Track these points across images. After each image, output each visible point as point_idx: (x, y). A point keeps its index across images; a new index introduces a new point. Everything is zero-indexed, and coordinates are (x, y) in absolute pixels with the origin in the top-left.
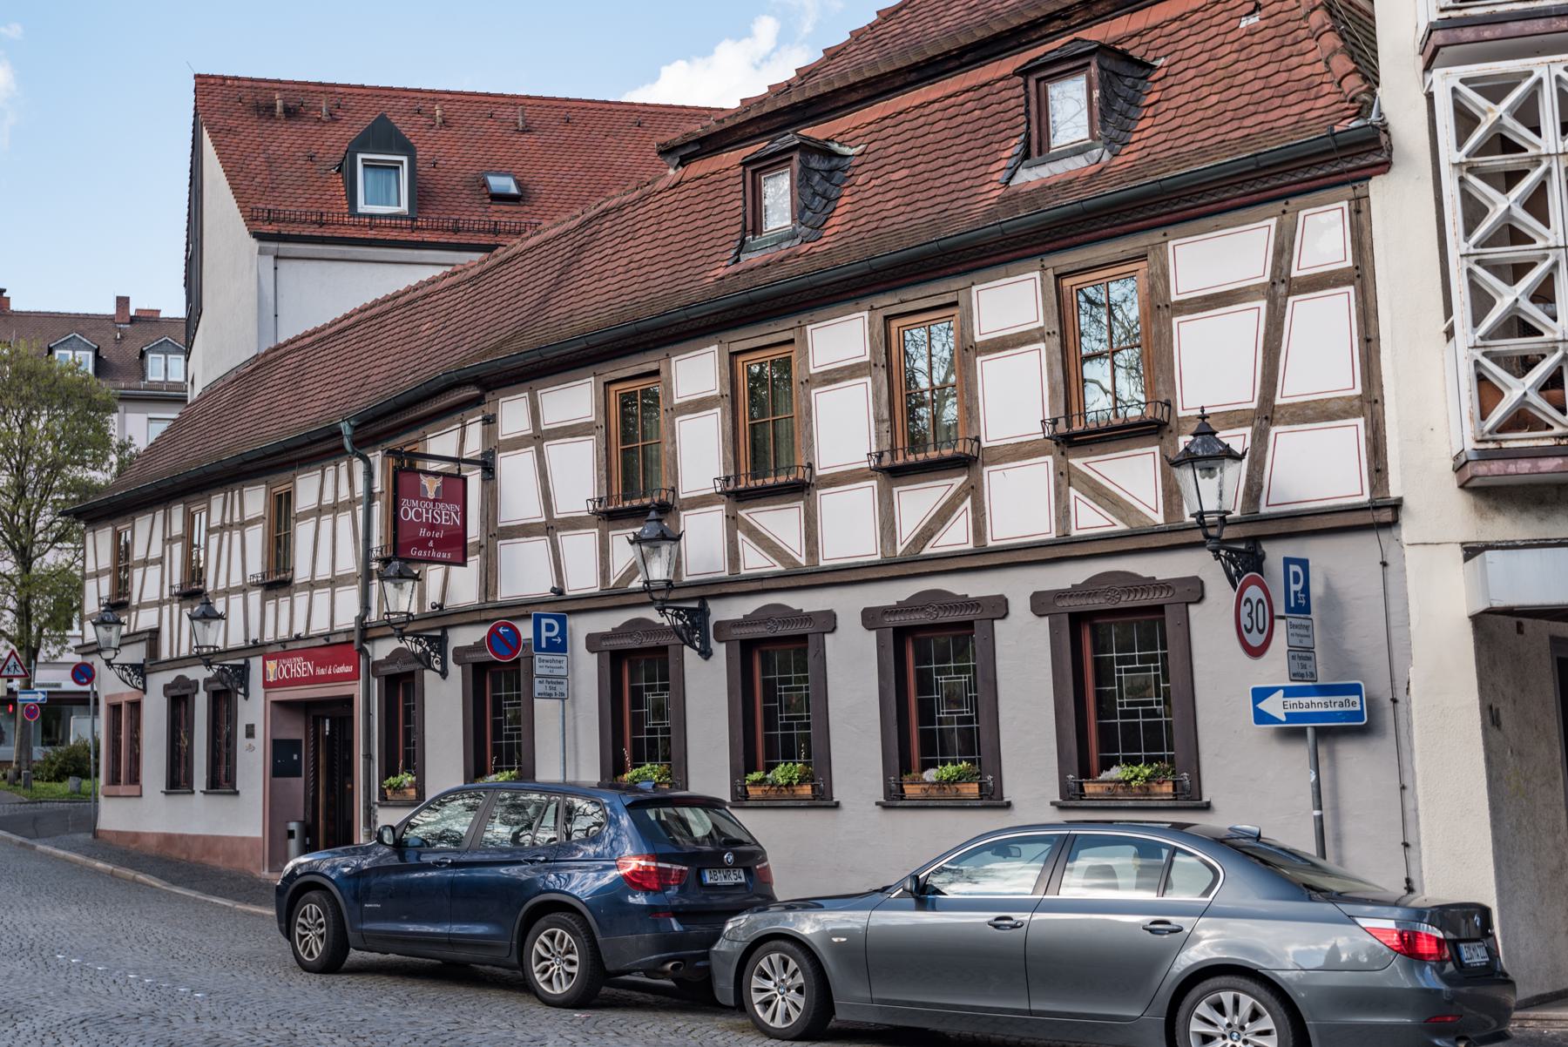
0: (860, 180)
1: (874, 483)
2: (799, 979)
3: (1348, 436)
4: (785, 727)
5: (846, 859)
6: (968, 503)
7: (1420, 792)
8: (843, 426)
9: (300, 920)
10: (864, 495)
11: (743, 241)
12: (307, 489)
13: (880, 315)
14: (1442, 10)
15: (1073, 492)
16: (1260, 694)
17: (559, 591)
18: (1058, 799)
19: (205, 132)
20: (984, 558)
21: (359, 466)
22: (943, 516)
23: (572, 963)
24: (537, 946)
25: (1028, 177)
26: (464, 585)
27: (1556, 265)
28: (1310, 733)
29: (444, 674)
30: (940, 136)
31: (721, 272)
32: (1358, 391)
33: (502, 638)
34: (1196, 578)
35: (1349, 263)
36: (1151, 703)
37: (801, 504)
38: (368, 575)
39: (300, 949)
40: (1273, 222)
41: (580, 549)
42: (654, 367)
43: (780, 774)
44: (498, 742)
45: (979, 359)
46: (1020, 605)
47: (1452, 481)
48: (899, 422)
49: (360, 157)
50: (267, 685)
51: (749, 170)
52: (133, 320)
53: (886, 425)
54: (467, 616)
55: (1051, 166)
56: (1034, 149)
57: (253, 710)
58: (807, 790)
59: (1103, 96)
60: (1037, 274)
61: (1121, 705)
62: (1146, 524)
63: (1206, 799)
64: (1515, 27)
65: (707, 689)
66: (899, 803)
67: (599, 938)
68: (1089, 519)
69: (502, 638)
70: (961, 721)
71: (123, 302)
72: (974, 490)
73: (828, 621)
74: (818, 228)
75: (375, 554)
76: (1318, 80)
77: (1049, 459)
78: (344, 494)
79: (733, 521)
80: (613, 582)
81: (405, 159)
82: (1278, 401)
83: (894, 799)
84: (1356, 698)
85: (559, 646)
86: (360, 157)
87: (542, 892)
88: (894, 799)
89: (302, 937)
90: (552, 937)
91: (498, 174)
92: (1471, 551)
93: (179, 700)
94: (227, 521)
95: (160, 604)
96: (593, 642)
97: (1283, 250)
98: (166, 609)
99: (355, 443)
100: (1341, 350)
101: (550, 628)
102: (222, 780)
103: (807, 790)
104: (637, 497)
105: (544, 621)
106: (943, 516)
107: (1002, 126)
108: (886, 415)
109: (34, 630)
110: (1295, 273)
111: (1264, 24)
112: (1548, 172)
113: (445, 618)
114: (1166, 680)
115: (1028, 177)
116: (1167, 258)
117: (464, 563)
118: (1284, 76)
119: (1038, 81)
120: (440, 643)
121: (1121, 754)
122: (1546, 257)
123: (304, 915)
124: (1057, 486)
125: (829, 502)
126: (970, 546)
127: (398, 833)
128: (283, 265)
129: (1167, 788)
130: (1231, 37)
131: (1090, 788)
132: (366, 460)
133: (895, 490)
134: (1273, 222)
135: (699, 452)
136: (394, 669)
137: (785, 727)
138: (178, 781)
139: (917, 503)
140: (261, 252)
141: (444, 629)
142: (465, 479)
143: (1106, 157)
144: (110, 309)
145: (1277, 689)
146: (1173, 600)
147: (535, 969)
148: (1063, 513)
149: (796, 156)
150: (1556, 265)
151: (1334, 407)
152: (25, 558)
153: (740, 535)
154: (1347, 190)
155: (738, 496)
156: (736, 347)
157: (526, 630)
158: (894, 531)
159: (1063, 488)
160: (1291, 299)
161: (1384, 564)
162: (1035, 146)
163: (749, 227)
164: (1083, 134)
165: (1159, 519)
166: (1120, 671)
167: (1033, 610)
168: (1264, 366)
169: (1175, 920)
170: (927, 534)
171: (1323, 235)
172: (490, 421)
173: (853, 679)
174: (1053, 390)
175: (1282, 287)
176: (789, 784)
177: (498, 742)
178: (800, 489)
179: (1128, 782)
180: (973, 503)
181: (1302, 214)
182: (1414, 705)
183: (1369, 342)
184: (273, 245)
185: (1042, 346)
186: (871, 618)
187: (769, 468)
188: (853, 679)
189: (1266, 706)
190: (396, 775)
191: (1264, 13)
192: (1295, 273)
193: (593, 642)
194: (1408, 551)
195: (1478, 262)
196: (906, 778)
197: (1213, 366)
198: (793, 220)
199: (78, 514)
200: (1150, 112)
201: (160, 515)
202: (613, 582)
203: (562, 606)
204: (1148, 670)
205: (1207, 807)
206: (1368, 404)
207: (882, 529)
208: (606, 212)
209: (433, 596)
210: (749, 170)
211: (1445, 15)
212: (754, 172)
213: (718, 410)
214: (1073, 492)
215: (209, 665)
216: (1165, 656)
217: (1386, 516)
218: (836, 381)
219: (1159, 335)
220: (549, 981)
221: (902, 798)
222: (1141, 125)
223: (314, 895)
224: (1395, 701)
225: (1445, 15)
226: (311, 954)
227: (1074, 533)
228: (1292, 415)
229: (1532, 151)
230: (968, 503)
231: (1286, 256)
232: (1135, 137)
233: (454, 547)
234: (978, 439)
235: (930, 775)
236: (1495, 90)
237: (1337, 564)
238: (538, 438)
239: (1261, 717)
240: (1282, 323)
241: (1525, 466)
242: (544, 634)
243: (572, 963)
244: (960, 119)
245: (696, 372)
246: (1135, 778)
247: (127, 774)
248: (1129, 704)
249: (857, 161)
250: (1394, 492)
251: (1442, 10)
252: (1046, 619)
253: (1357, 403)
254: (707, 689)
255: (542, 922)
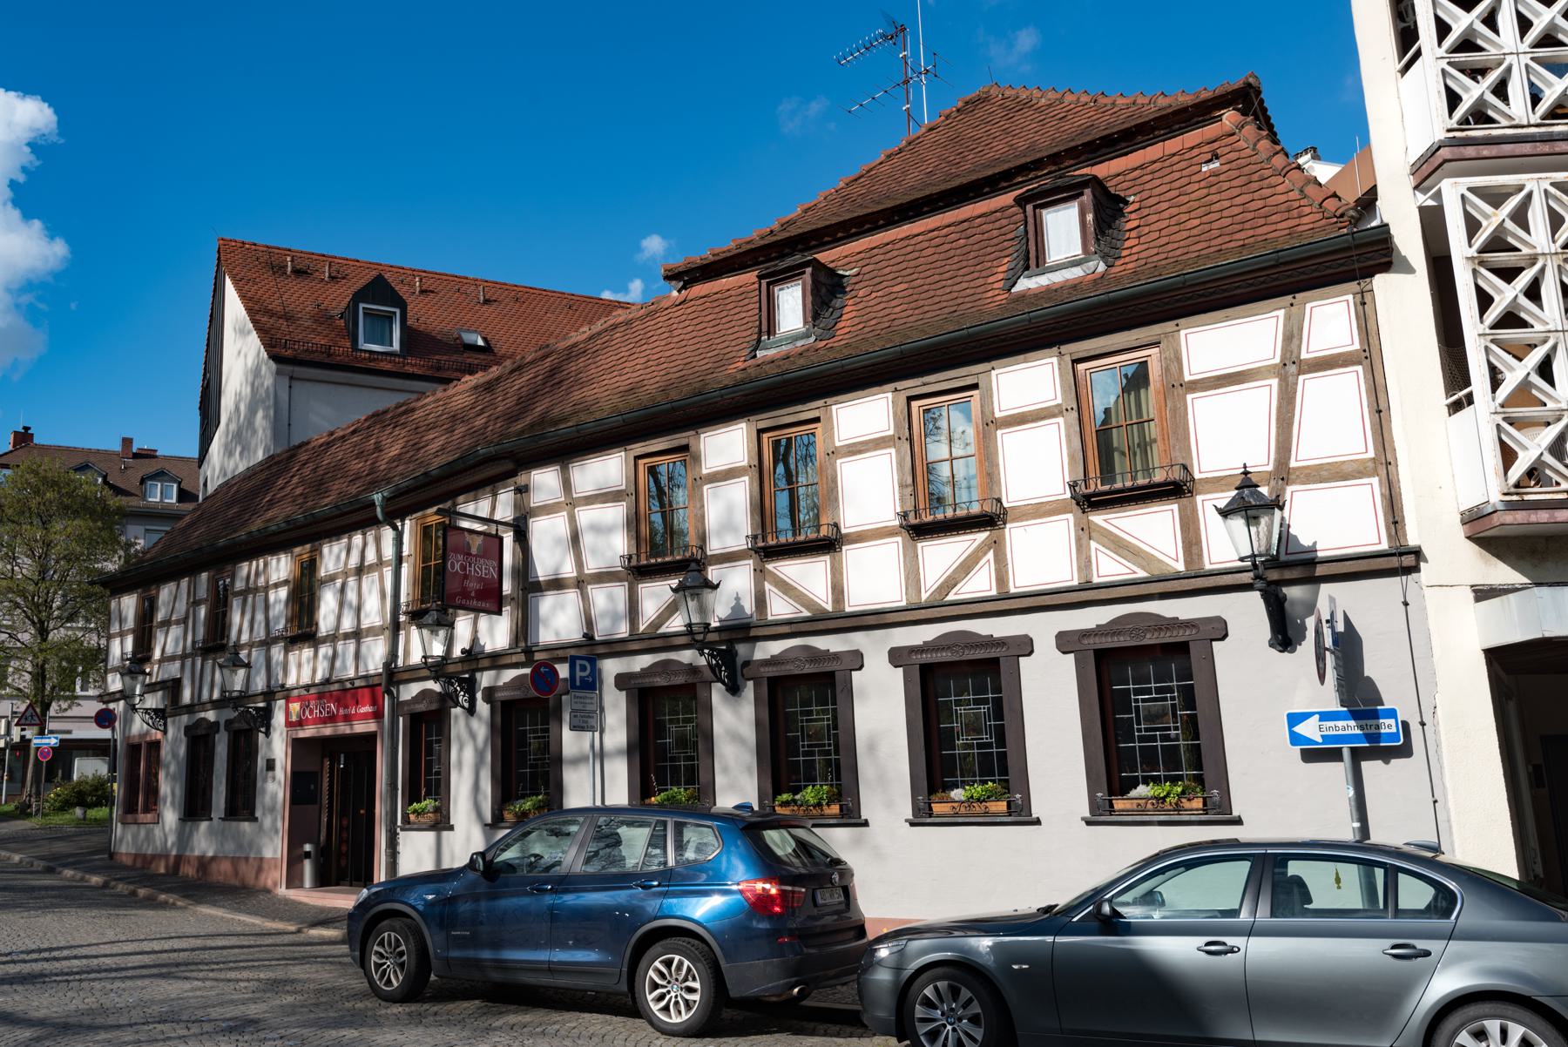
0: (861, 293)
1: (899, 539)
2: (976, 1009)
3: (1363, 497)
4: (806, 754)
5: (915, 876)
6: (990, 555)
7: (1451, 804)
8: (868, 491)
9: (376, 948)
10: (892, 549)
11: (759, 341)
12: (333, 557)
13: (903, 397)
14: (1449, 131)
15: (1093, 544)
16: (1295, 719)
17: (589, 637)
18: (1087, 815)
19: (228, 282)
20: (1007, 603)
21: (388, 534)
22: (966, 567)
23: (691, 990)
24: (651, 973)
25: (1025, 284)
26: (496, 633)
27: (1554, 348)
28: (1346, 754)
29: (471, 711)
30: (930, 259)
31: (741, 365)
32: (1371, 454)
33: (543, 675)
34: (1026, 636)
35: (1357, 346)
36: (1169, 729)
37: (827, 558)
38: (396, 627)
39: (376, 977)
40: (1281, 313)
41: (607, 600)
42: (684, 442)
43: (809, 794)
44: (526, 774)
45: (999, 432)
46: (1045, 644)
47: (1459, 532)
48: (920, 487)
49: (361, 306)
50: (289, 724)
51: (764, 282)
52: (136, 456)
53: (910, 489)
54: (497, 660)
55: (1050, 275)
56: (1032, 262)
57: (277, 746)
58: (835, 809)
59: (1096, 219)
60: (1055, 360)
61: (1139, 730)
62: (1166, 571)
63: (1235, 813)
64: (1507, 149)
65: (734, 723)
66: (929, 820)
67: (723, 963)
68: (1109, 568)
69: (543, 675)
70: (980, 746)
71: (127, 442)
72: (997, 545)
73: (1025, 646)
74: (830, 331)
75: (403, 608)
76: (1296, 204)
77: (1070, 516)
78: (371, 557)
79: (760, 573)
80: (642, 628)
81: (398, 311)
82: (1293, 464)
83: (922, 816)
84: (1392, 721)
85: (592, 683)
86: (361, 306)
87: (656, 918)
88: (922, 816)
89: (378, 966)
90: (668, 963)
91: (468, 331)
92: (1483, 594)
93: (199, 739)
94: (251, 584)
95: (183, 657)
96: (622, 681)
97: (1292, 336)
98: (188, 662)
99: (385, 514)
100: (1339, 423)
101: (583, 668)
102: (242, 804)
103: (835, 809)
104: (665, 552)
105: (578, 662)
106: (966, 567)
107: (989, 250)
108: (910, 481)
109: (48, 688)
110: (1304, 356)
111: (1225, 168)
112: (1543, 270)
113: (475, 657)
114: (836, 728)
115: (1025, 284)
116: (1179, 344)
117: (499, 613)
118: (1260, 204)
119: (1035, 207)
120: (470, 686)
121: (1139, 774)
122: (1545, 341)
123: (381, 944)
124: (1078, 540)
125: (851, 555)
126: (994, 592)
127: (488, 857)
128: (296, 384)
129: (1197, 803)
130: (1194, 178)
131: (1119, 804)
132: (395, 528)
133: (920, 545)
134: (1281, 313)
135: (725, 515)
136: (421, 707)
137: (806, 754)
138: (195, 808)
139: (941, 555)
140: (278, 373)
141: (473, 672)
142: (501, 539)
143: (1102, 267)
144: (117, 447)
145: (1312, 714)
146: (1199, 636)
147: (650, 997)
148: (1085, 562)
149: (809, 270)
150: (1554, 348)
151: (1348, 469)
152: (43, 632)
153: (767, 586)
154: (1353, 286)
155: (767, 550)
156: (762, 425)
157: (563, 671)
158: (919, 581)
159: (1084, 541)
160: (1301, 378)
161: (1406, 604)
162: (1032, 256)
163: (764, 328)
164: (1077, 250)
165: (1180, 567)
166: (1136, 701)
167: (890, 662)
168: (1278, 434)
169: (1421, 944)
170: (950, 583)
171: (1329, 320)
172: (522, 490)
173: (881, 712)
174: (1072, 457)
175: (1292, 367)
176: (819, 805)
177: (526, 774)
178: (829, 545)
179: (1164, 799)
180: (996, 556)
181: (1308, 306)
182: (1441, 728)
183: (1379, 412)
184: (289, 368)
185: (1060, 420)
186: (1065, 642)
187: (796, 526)
188: (881, 712)
189: (1300, 729)
190: (419, 801)
191: (1223, 160)
192: (1304, 356)
193: (622, 681)
194: (1427, 591)
195: (1492, 341)
196: (933, 797)
197: (1225, 436)
198: (805, 322)
199: (293, 452)
200: (1133, 234)
201: (184, 583)
202: (642, 628)
203: (590, 650)
204: (1165, 699)
205: (1238, 822)
206: (1383, 464)
207: (907, 579)
208: (615, 326)
209: (462, 642)
210: (764, 282)
211: (1451, 135)
212: (769, 284)
213: (746, 478)
214: (1093, 544)
215: (235, 708)
216: (835, 710)
217: (1408, 561)
218: (860, 452)
219: (1174, 410)
220: (666, 1009)
221: (930, 816)
222: (1127, 244)
223: (397, 923)
224: (1423, 724)
225: (1451, 135)
226: (389, 982)
227: (1096, 580)
228: (1308, 476)
229: (1525, 251)
230: (990, 555)
231: (1295, 341)
232: (1125, 253)
233: (489, 600)
234: (999, 501)
235: (958, 794)
236: (1495, 198)
237: (1362, 604)
238: (571, 502)
239: (1295, 739)
240: (1294, 398)
241: (1543, 516)
242: (579, 674)
243: (691, 990)
244: (946, 247)
245: (727, 446)
246: (1168, 795)
247: (141, 798)
248: (1147, 730)
249: (854, 280)
250: (1412, 540)
251: (1449, 131)
252: (1072, 656)
253: (1371, 465)
254: (734, 723)
255: (657, 948)
